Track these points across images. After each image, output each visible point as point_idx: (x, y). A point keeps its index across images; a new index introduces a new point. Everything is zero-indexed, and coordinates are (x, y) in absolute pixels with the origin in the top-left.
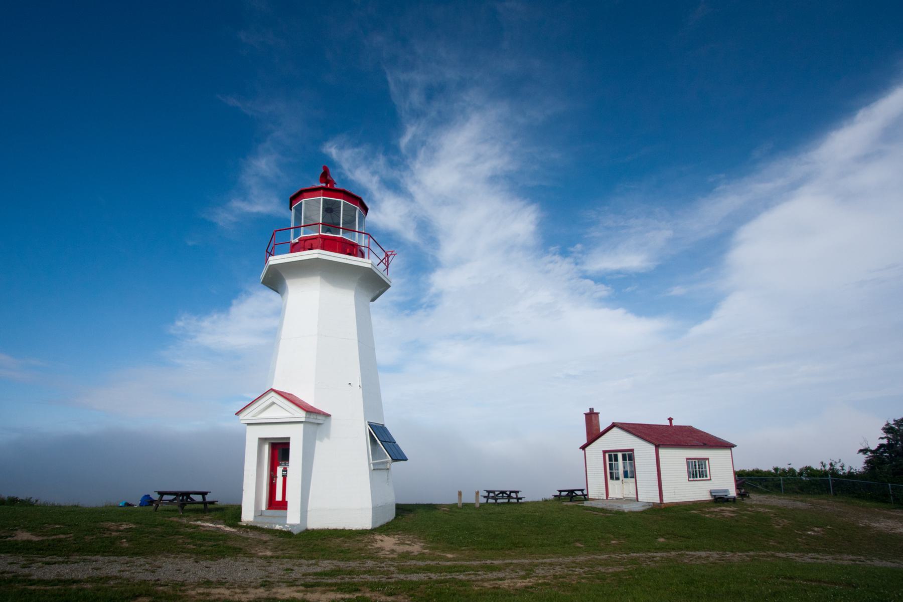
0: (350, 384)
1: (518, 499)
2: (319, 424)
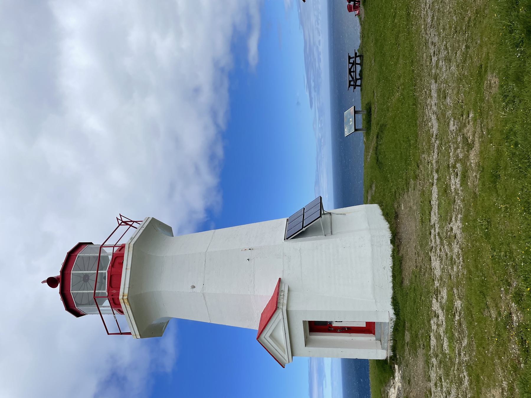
0: (248, 260)
1: (356, 56)
2: (289, 290)
